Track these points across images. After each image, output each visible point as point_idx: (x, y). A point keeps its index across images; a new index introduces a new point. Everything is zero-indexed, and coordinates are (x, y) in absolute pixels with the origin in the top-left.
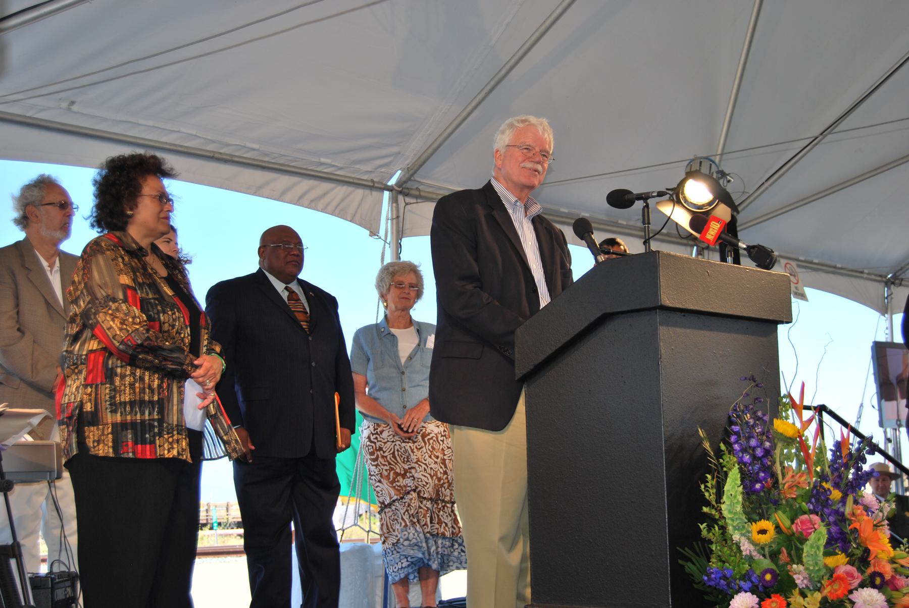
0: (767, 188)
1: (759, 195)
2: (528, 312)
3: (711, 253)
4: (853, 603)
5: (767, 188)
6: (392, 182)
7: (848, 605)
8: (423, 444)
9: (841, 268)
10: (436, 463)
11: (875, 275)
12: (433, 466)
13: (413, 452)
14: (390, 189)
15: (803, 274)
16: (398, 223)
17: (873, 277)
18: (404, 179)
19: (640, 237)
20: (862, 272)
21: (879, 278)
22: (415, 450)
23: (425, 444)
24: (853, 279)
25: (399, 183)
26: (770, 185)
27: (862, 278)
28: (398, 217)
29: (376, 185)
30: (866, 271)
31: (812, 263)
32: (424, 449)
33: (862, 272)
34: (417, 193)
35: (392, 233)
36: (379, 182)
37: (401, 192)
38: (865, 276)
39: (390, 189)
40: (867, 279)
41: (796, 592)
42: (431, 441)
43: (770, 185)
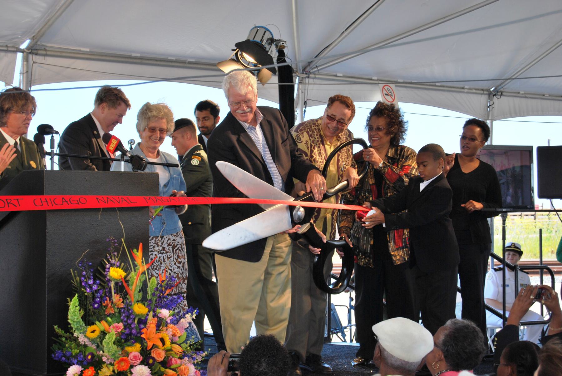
0: (346, 36)
1: (341, 41)
2: (203, 136)
3: (34, 56)
4: (132, 373)
5: (346, 36)
6: (23, 46)
7: (129, 375)
8: (172, 254)
9: (377, 80)
10: (179, 267)
11: (476, 89)
12: (176, 270)
13: (164, 261)
14: (22, 51)
15: (398, 91)
16: (27, 77)
17: (474, 91)
18: (31, 45)
19: (486, 94)
20: (463, 88)
21: (482, 92)
22: (166, 260)
23: (174, 254)
24: (454, 94)
25: (28, 48)
26: (348, 34)
27: (463, 92)
28: (27, 72)
29: (10, 49)
30: (466, 87)
31: (371, 79)
32: (172, 259)
33: (463, 88)
34: (44, 52)
35: (23, 84)
36: (13, 47)
37: (30, 53)
38: (466, 90)
39: (22, 51)
40: (467, 93)
41: (104, 366)
42: (178, 251)
43: (348, 34)
